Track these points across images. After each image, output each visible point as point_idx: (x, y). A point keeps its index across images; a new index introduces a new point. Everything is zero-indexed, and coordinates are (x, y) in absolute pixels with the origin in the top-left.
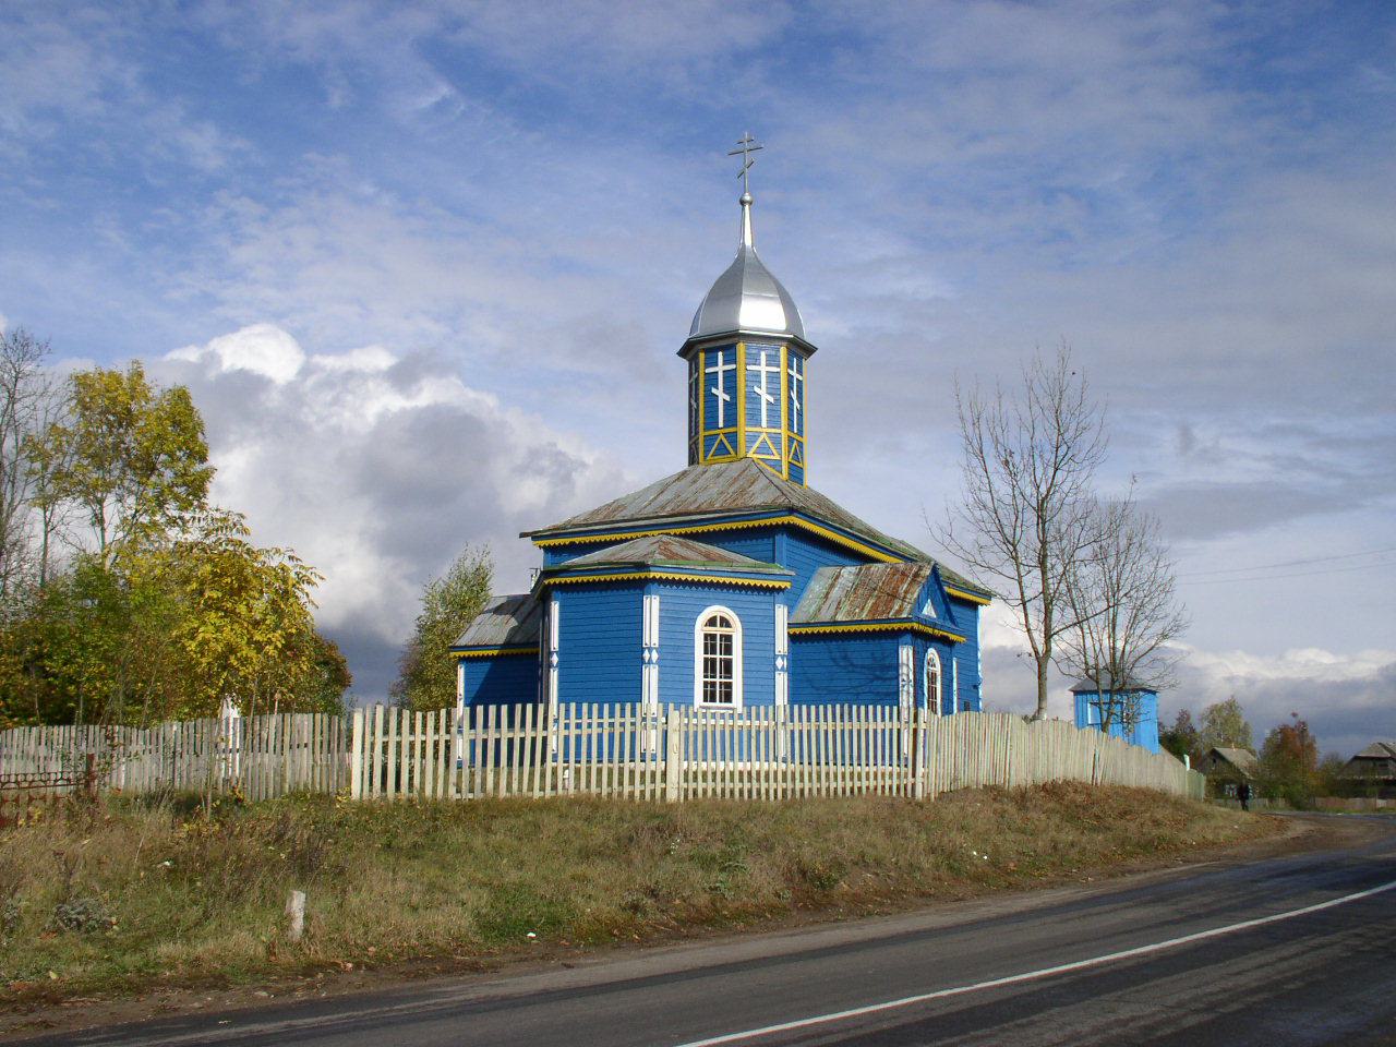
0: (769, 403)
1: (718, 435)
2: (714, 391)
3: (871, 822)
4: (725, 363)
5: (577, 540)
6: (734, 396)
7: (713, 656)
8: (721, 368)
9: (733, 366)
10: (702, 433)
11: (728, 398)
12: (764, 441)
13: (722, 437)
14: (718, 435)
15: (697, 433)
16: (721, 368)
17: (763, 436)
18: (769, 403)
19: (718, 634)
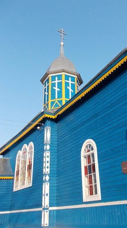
0: (55, 87)
1: (55, 101)
2: (59, 90)
3: (39, 131)
4: (58, 80)
5: (60, 113)
6: (48, 93)
7: (92, 185)
8: (56, 81)
9: (52, 82)
10: (50, 101)
11: (68, 87)
12: (57, 103)
13: (56, 101)
14: (55, 101)
15: (48, 100)
16: (56, 81)
17: (56, 101)
18: (55, 87)
19: (94, 184)
